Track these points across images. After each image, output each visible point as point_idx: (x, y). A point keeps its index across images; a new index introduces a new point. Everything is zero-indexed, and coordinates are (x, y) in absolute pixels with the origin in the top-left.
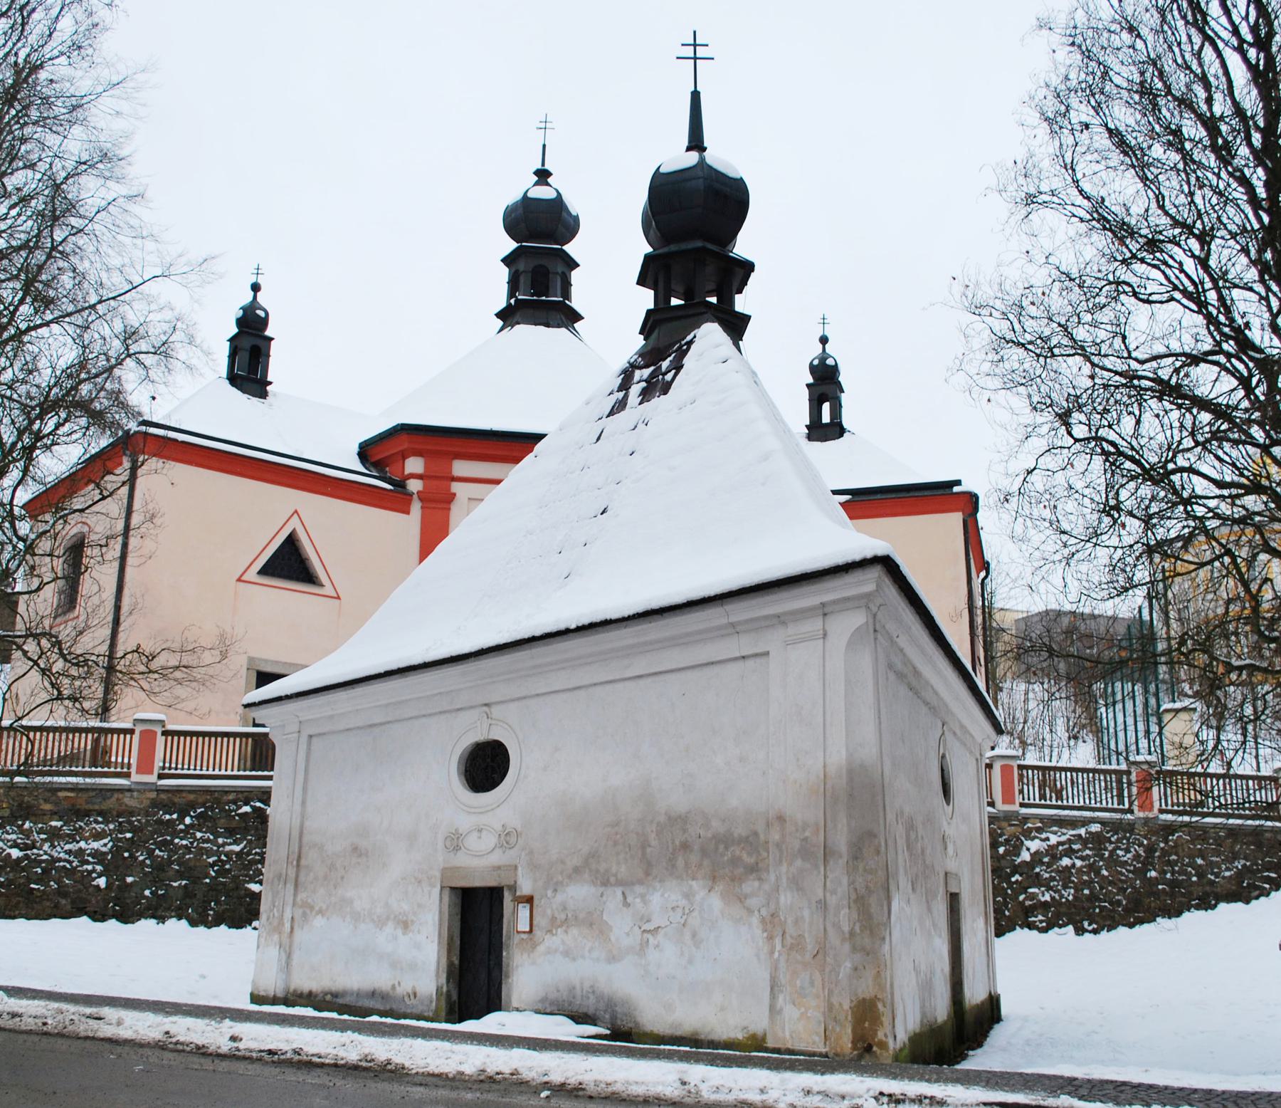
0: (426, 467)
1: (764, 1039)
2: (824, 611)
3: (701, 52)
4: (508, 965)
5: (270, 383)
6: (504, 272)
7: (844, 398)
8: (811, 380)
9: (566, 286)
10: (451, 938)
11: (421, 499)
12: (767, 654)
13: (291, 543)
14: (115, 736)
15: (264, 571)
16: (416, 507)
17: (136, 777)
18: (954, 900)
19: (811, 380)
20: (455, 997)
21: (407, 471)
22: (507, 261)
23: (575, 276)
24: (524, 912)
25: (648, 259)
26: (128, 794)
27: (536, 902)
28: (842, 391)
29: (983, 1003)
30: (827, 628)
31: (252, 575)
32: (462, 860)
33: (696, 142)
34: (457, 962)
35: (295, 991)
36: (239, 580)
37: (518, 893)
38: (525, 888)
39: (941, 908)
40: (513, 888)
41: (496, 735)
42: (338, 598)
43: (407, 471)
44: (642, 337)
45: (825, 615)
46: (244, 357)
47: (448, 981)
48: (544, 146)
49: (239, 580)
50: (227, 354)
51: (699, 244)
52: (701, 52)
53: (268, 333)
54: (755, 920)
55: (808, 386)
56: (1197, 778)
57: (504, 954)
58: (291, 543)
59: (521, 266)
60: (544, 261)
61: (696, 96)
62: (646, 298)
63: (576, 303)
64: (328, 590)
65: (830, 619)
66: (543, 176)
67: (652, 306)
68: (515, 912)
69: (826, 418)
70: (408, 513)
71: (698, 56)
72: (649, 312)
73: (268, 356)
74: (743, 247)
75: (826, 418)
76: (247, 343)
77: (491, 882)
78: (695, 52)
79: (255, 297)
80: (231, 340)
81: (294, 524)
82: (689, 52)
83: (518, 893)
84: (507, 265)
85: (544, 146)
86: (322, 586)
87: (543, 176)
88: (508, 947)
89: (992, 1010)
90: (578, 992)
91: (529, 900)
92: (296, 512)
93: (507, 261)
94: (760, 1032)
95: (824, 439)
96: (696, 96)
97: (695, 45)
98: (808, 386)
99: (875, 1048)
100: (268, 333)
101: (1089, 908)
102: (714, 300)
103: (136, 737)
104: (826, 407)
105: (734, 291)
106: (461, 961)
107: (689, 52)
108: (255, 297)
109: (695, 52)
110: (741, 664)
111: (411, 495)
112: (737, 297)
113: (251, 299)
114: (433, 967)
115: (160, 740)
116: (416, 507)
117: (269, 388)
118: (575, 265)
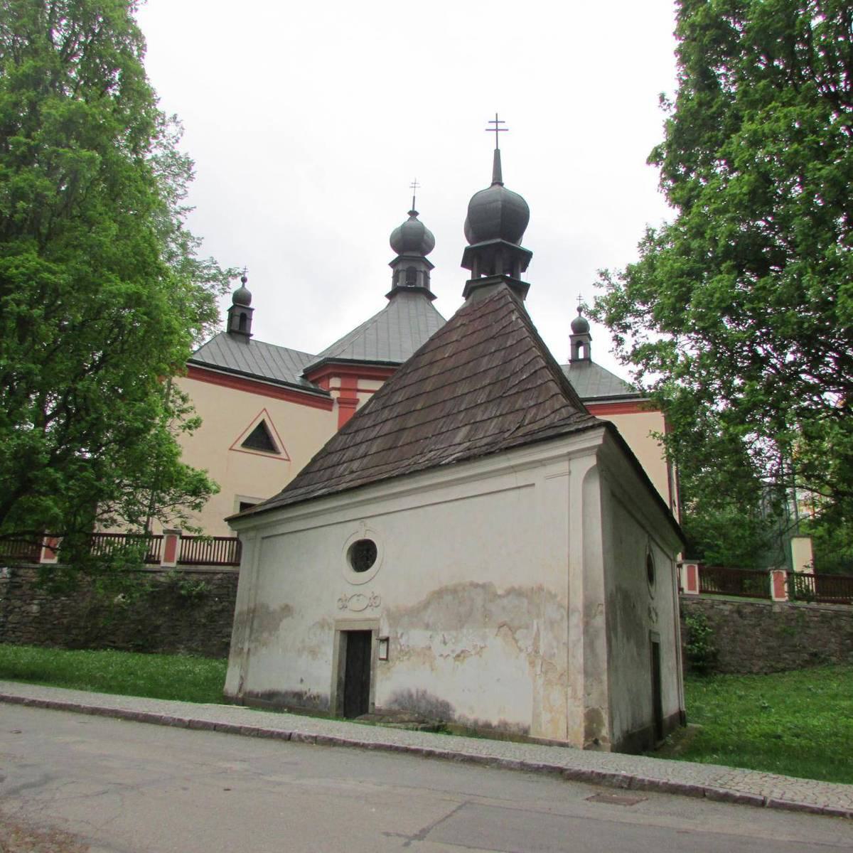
0: (342, 383)
1: (526, 731)
2: (570, 456)
3: (500, 126)
4: (373, 680)
5: (252, 335)
6: (390, 271)
7: (592, 344)
8: (572, 333)
9: (427, 278)
10: (340, 662)
11: (339, 403)
12: (533, 485)
13: (262, 427)
14: (155, 540)
15: (246, 444)
16: (336, 408)
17: (163, 564)
18: (655, 648)
19: (572, 333)
20: (342, 700)
21: (331, 386)
22: (393, 264)
23: (432, 273)
24: (383, 647)
25: (467, 251)
26: (159, 574)
27: (391, 641)
28: (591, 339)
29: (675, 714)
30: (571, 469)
31: (238, 446)
32: (347, 615)
33: (497, 180)
34: (343, 678)
35: (249, 693)
36: (230, 449)
37: (381, 635)
38: (385, 633)
39: (647, 652)
40: (378, 631)
41: (368, 537)
42: (289, 460)
43: (331, 386)
44: (464, 298)
45: (570, 460)
46: (237, 320)
47: (338, 690)
48: (414, 197)
49: (230, 449)
50: (253, 321)
51: (499, 240)
52: (500, 126)
53: (251, 306)
54: (523, 655)
55: (571, 336)
56: (803, 578)
57: (371, 673)
58: (262, 427)
59: (400, 267)
60: (414, 264)
61: (497, 153)
62: (467, 275)
63: (433, 289)
64: (283, 455)
65: (571, 462)
66: (413, 214)
67: (470, 278)
68: (378, 646)
69: (581, 356)
70: (331, 410)
71: (499, 132)
72: (468, 282)
73: (251, 319)
74: (526, 243)
75: (581, 356)
76: (238, 312)
77: (364, 627)
78: (497, 126)
79: (243, 286)
80: (229, 310)
81: (264, 416)
82: (493, 126)
83: (381, 635)
84: (392, 267)
85: (414, 197)
86: (279, 453)
87: (413, 214)
88: (374, 668)
89: (399, 262)
90: (415, 697)
91: (387, 640)
92: (265, 409)
93: (393, 264)
94: (526, 725)
95: (580, 367)
96: (497, 153)
97: (497, 122)
98: (571, 336)
99: (600, 742)
100: (251, 306)
101: (823, 557)
102: (509, 275)
103: (163, 541)
104: (581, 350)
105: (520, 269)
106: (346, 676)
107: (493, 126)
108: (243, 286)
109: (497, 126)
110: (517, 491)
111: (332, 400)
112: (522, 274)
113: (241, 286)
114: (329, 681)
115: (179, 541)
116: (336, 408)
117: (251, 338)
118: (431, 266)
